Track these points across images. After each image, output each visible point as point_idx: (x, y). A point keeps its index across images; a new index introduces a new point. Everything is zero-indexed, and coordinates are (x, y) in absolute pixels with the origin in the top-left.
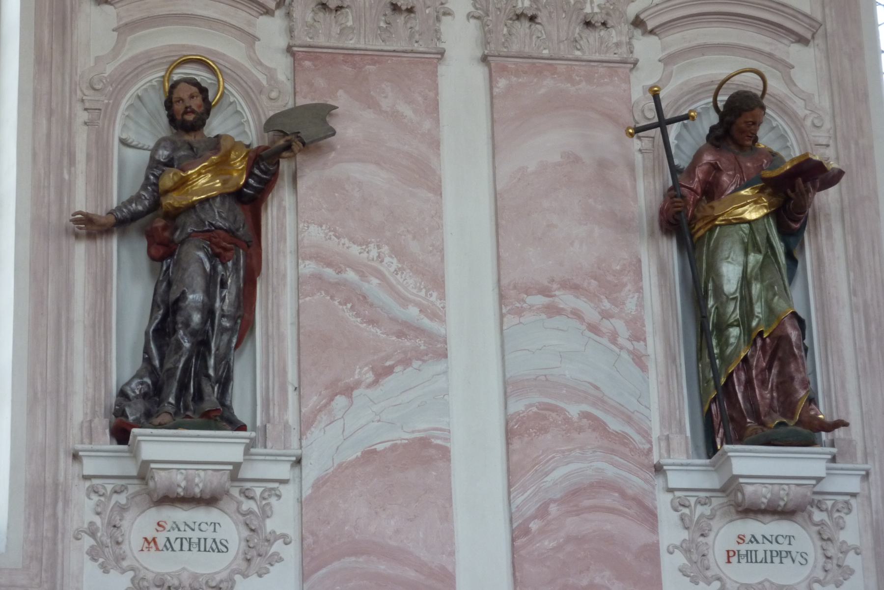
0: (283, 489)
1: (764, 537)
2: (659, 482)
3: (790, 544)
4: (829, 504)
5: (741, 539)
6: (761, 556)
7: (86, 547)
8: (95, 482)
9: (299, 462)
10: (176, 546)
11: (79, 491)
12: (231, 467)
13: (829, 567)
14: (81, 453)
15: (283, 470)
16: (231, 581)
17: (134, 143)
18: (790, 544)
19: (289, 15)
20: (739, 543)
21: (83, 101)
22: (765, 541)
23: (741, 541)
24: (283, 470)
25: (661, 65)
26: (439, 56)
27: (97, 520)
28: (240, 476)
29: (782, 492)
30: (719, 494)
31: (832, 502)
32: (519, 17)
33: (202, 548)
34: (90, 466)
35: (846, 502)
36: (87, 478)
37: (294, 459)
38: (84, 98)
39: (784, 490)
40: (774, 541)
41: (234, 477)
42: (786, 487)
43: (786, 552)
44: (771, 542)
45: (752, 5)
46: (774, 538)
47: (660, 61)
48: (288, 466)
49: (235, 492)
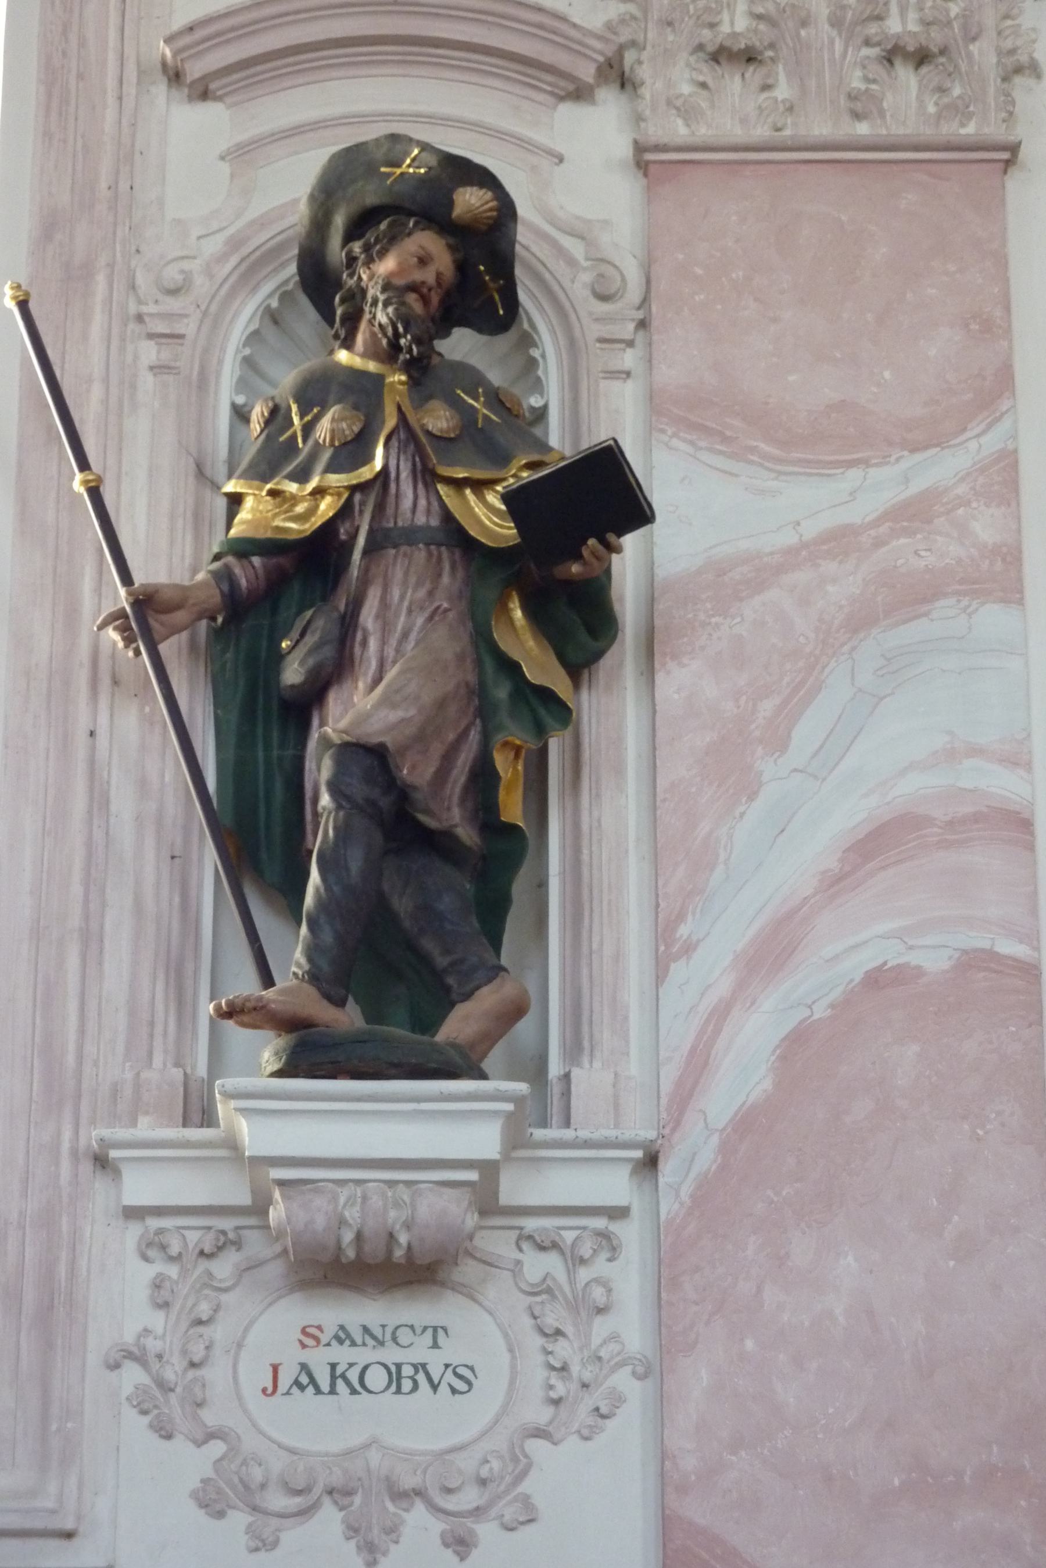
1: (366, 1330)
2: (101, 1185)
5: (309, 1335)
6: (377, 1378)
7: (128, 1389)
8: (154, 1223)
9: (651, 1162)
12: (473, 1176)
14: (113, 1154)
15: (613, 1185)
17: (508, 405)
20: (304, 1346)
21: (140, 318)
23: (310, 1342)
24: (613, 1185)
25: (225, 168)
26: (1006, 156)
27: (157, 1321)
28: (504, 1200)
29: (392, 1214)
34: (140, 1187)
36: (134, 1213)
37: (638, 1154)
38: (144, 309)
39: (397, 1204)
41: (487, 1202)
42: (404, 1193)
43: (415, 1367)
45: (313, 14)
46: (389, 1331)
47: (222, 158)
48: (625, 1171)
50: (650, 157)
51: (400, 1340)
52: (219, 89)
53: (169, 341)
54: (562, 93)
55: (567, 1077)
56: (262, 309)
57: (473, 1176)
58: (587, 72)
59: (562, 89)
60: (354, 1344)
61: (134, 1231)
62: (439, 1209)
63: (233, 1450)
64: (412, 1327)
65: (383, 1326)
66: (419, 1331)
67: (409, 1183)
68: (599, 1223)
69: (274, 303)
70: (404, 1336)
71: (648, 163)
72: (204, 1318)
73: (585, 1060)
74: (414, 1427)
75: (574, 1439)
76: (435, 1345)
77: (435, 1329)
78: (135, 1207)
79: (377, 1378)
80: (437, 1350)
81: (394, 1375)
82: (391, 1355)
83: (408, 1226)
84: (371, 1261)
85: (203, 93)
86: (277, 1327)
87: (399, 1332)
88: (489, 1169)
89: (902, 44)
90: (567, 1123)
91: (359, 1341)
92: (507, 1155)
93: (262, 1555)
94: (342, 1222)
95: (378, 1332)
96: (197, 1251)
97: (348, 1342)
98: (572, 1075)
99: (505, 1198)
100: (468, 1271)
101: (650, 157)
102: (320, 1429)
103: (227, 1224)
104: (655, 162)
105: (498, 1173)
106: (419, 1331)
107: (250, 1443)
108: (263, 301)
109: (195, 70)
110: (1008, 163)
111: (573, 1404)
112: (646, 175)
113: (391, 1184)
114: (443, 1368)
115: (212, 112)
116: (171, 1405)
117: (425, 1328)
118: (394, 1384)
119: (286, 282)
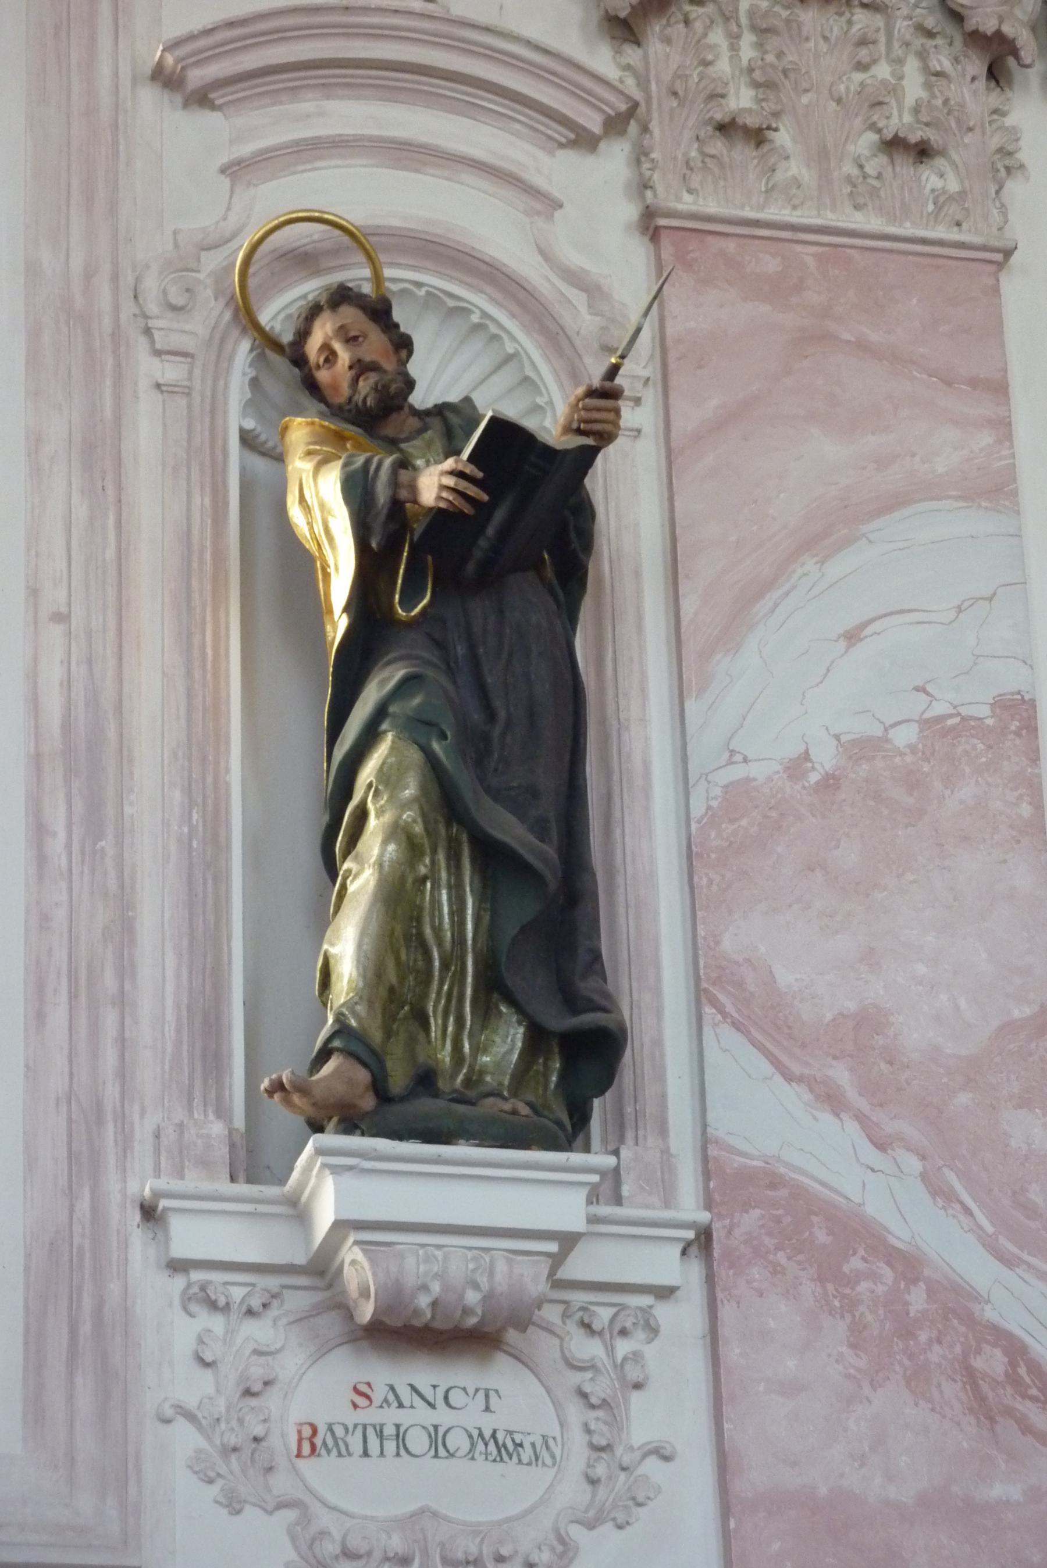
0: (663, 1312)
3: (487, 1409)
4: (604, 1315)
6: (418, 1441)
8: (197, 1276)
10: (355, 1442)
11: (958, 1344)
13: (600, 1470)
16: (565, 1548)
18: (487, 1409)
19: (640, 155)
22: (417, 1401)
23: (361, 1401)
24: (663, 1264)
30: (302, 1281)
31: (612, 1311)
32: (726, 128)
33: (442, 1452)
34: (189, 1237)
35: (646, 1311)
36: (178, 1266)
40: (440, 1402)
44: (432, 1406)
46: (440, 1392)
49: (551, 1314)
50: (662, 222)
51: (453, 1401)
52: (218, 98)
54: (564, 140)
58: (593, 122)
59: (565, 137)
60: (401, 1405)
61: (179, 1282)
64: (464, 1389)
65: (435, 1387)
66: (471, 1391)
67: (439, 1247)
70: (456, 1398)
71: (657, 229)
72: (594, 1327)
73: (630, 1135)
79: (418, 1441)
80: (435, 1423)
81: (437, 1439)
82: (443, 1417)
85: (202, 99)
86: (320, 1386)
87: (451, 1394)
88: (568, 1241)
89: (901, 135)
91: (406, 1402)
95: (428, 1393)
96: (244, 1309)
97: (396, 1404)
103: (272, 1282)
104: (665, 227)
106: (471, 1391)
109: (197, 77)
110: (1000, 266)
115: (211, 119)
117: (477, 1390)
118: (433, 1449)
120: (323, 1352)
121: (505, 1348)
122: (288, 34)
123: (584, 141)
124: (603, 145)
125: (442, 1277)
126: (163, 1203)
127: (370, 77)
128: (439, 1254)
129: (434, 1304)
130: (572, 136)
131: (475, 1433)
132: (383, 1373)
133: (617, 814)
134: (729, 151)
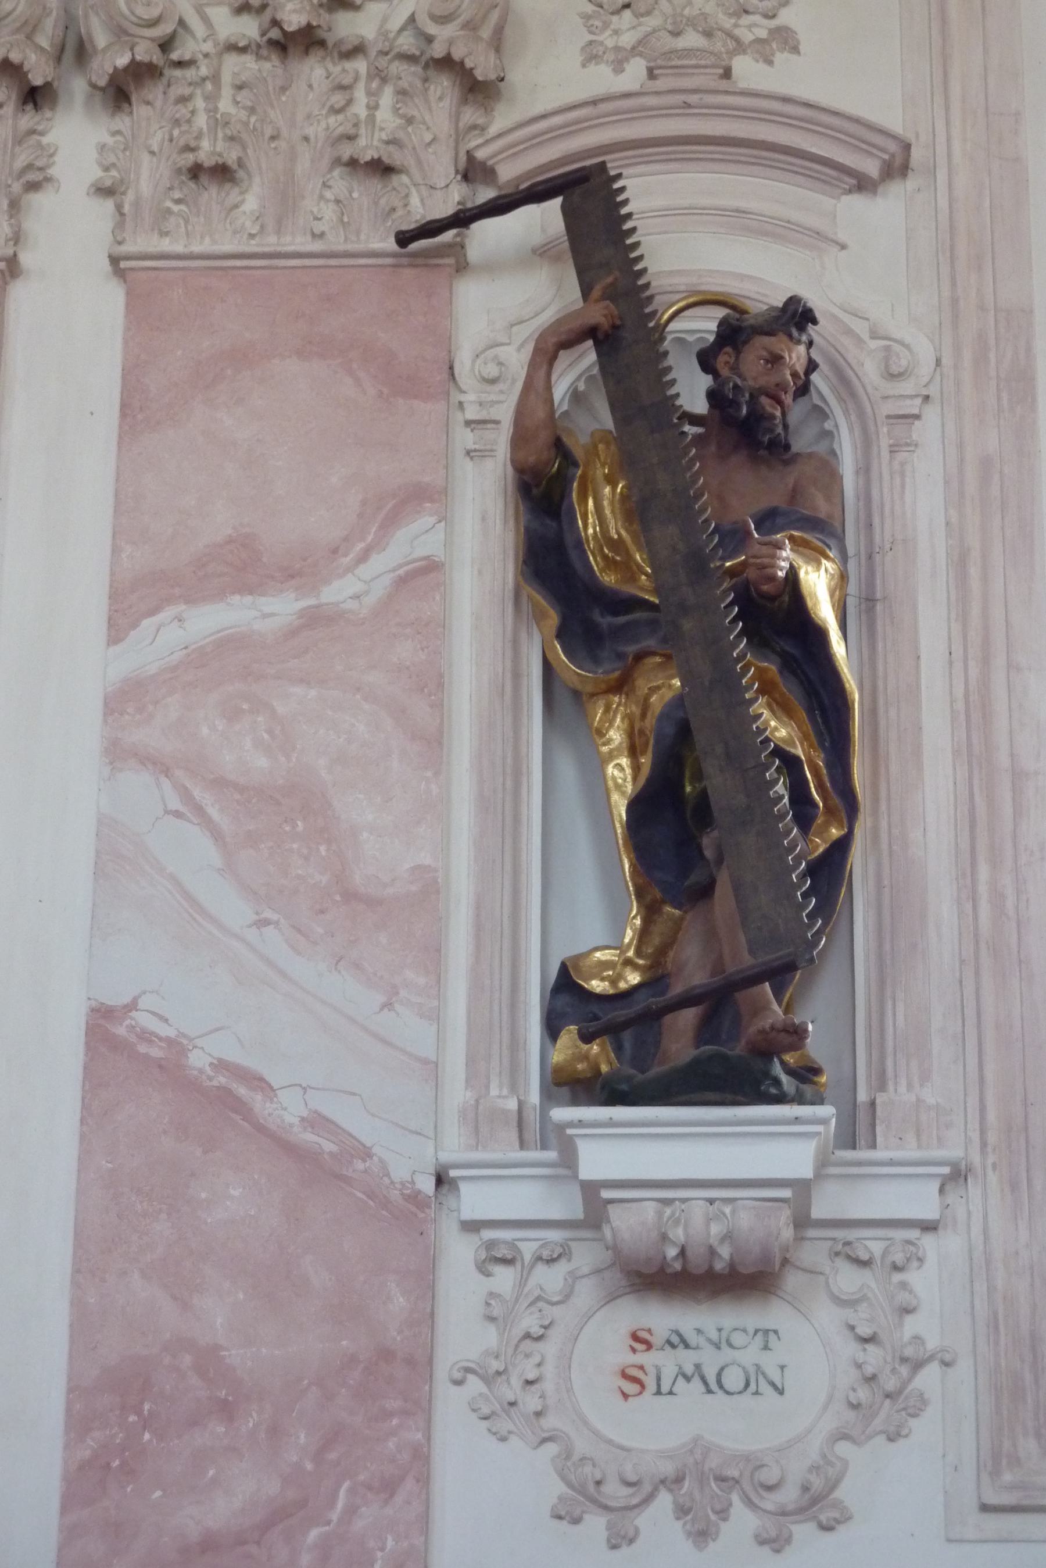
8: (488, 1234)
12: (786, 1193)
15: (920, 1200)
36: (472, 1227)
50: (123, 264)
53: (900, 421)
55: (873, 1104)
56: (571, 390)
57: (786, 1193)
58: (871, 168)
62: (754, 1224)
63: (568, 1453)
68: (913, 1234)
69: (582, 386)
74: (734, 1427)
75: (881, 1439)
76: (766, 1348)
77: (766, 1332)
78: (584, 1200)
83: (728, 1237)
84: (695, 1271)
86: (606, 1331)
88: (802, 1188)
90: (873, 1146)
92: (819, 1176)
93: (625, 1550)
94: (664, 1237)
98: (878, 1101)
99: (817, 1212)
100: (792, 1280)
101: (123, 264)
102: (657, 1430)
103: (554, 1235)
104: (132, 269)
105: (810, 1191)
106: (751, 1331)
107: (582, 1446)
108: (572, 384)
111: (882, 1402)
112: (125, 281)
113: (711, 1201)
114: (630, 1399)
116: (514, 1409)
119: (588, 369)
120: (611, 1298)
121: (781, 1294)
122: (764, 162)
123: (863, 184)
124: (880, 189)
125: (701, 1229)
126: (453, 1173)
127: (634, 157)
128: (727, 1210)
129: (683, 1252)
130: (854, 182)
131: (752, 1370)
132: (662, 1317)
133: (524, 750)
134: (152, 40)
